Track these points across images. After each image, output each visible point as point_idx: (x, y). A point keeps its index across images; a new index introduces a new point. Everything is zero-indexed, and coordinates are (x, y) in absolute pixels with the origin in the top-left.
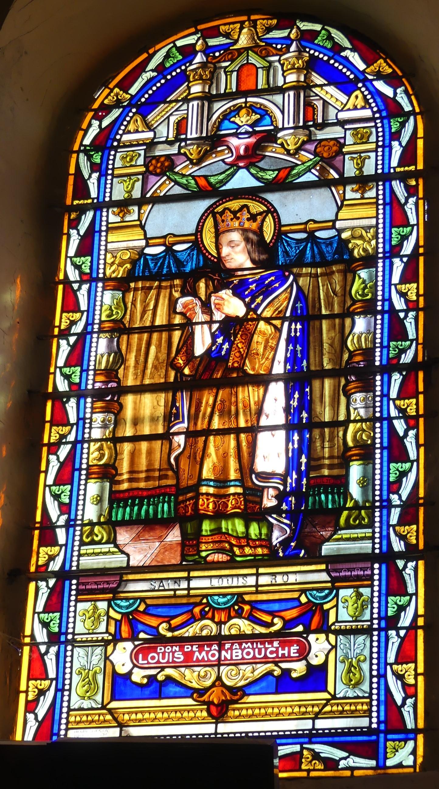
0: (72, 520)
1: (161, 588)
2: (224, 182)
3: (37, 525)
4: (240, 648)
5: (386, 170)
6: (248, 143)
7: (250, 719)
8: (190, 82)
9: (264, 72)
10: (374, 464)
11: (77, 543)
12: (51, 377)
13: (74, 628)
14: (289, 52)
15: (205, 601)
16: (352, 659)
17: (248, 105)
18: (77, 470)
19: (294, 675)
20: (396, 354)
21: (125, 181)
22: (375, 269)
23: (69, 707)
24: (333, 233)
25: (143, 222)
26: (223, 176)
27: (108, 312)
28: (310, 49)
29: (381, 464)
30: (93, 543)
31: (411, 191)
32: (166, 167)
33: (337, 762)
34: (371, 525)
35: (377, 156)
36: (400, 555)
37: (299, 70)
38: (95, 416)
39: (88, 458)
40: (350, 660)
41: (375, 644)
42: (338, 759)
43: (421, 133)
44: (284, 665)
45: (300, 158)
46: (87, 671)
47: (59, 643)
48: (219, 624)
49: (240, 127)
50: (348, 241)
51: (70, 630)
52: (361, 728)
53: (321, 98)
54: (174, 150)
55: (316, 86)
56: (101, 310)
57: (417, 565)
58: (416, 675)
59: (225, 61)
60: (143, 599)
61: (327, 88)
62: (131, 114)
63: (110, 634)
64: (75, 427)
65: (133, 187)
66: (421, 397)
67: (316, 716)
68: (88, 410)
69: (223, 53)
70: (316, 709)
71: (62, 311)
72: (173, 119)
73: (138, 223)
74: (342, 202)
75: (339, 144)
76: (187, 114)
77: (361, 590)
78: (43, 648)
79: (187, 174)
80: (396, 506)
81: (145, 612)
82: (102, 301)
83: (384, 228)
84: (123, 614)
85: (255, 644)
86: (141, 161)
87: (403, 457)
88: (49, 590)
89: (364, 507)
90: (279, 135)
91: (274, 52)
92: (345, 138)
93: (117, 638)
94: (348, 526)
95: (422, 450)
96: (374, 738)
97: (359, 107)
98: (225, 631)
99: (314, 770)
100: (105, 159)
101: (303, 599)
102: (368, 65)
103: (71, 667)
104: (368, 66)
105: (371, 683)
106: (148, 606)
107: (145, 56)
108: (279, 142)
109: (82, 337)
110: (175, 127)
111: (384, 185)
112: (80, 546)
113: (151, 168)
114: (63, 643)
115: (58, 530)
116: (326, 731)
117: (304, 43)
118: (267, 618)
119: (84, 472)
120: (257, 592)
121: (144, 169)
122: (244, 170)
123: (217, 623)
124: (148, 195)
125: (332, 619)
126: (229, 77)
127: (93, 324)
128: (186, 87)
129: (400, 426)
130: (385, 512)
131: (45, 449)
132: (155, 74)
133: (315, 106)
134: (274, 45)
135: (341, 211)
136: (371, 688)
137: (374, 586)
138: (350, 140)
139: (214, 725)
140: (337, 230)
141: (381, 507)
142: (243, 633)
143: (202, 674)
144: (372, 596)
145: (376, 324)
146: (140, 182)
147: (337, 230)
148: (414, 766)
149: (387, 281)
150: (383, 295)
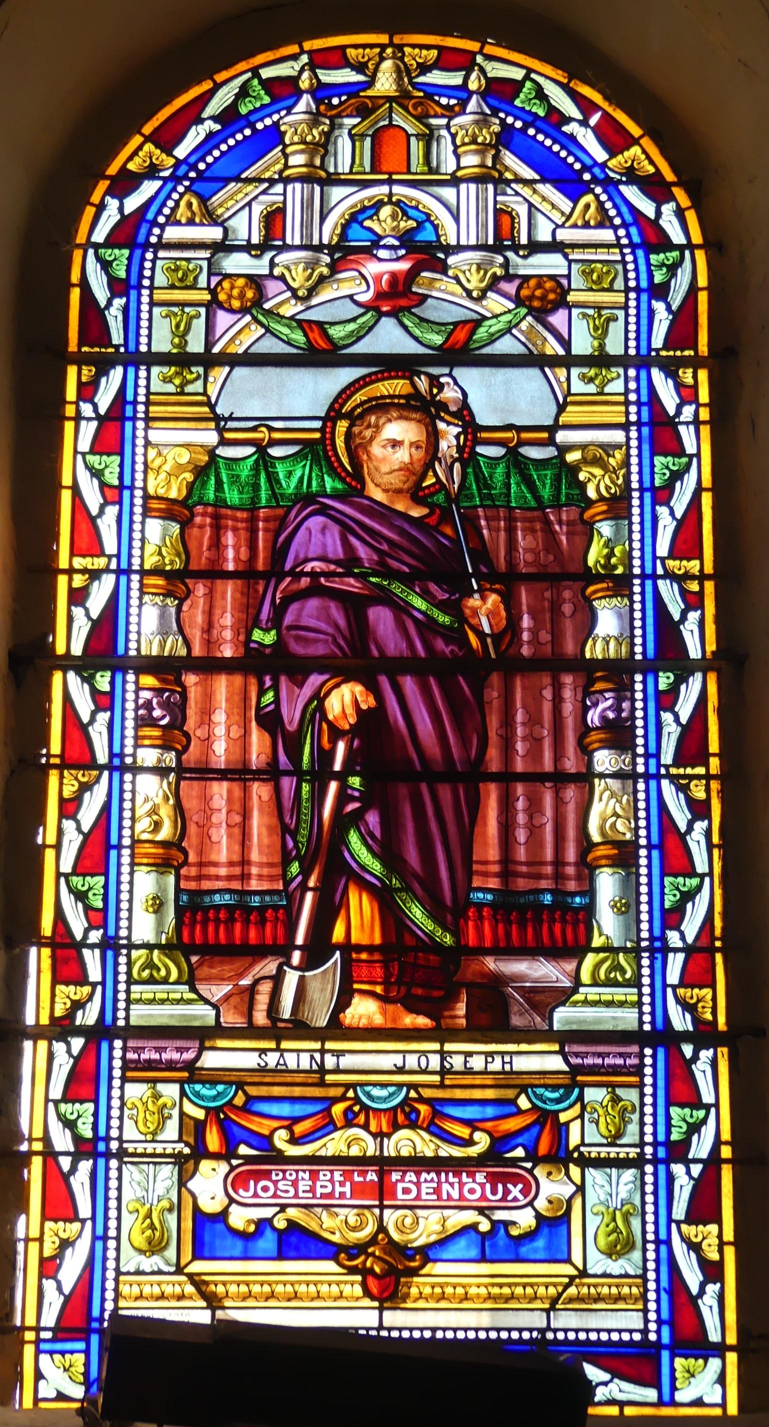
5: (644, 351)
9: (421, 143)
13: (120, 1128)
14: (463, 112)
17: (394, 199)
18: (114, 847)
21: (176, 315)
26: (352, 327)
29: (649, 875)
30: (152, 981)
35: (627, 315)
36: (685, 1036)
39: (132, 828)
43: (702, 281)
44: (499, 1215)
46: (148, 1206)
47: (95, 1155)
48: (379, 1135)
51: (114, 1133)
53: (525, 199)
54: (260, 267)
55: (519, 180)
57: (715, 1054)
58: (722, 1244)
61: (539, 187)
64: (99, 988)
68: (129, 742)
69: (346, 101)
70: (552, 1291)
72: (257, 209)
73: (204, 398)
74: (565, 398)
76: (285, 202)
78: (65, 1163)
80: (676, 950)
84: (208, 1110)
86: (203, 281)
89: (624, 950)
91: (438, 110)
92: (568, 277)
93: (200, 1152)
97: (592, 223)
98: (390, 1150)
100: (135, 266)
101: (523, 1103)
103: (119, 1199)
104: (612, 154)
106: (250, 1099)
108: (450, 273)
113: (222, 297)
114: (102, 1155)
115: (86, 952)
118: (463, 1132)
121: (209, 297)
123: (375, 1136)
124: (216, 350)
125: (574, 1140)
126: (357, 144)
128: (280, 154)
132: (218, 127)
133: (514, 213)
134: (437, 98)
136: (645, 1260)
137: (649, 1311)
138: (577, 281)
141: (652, 950)
142: (422, 1155)
144: (642, 1104)
150: (641, 481)
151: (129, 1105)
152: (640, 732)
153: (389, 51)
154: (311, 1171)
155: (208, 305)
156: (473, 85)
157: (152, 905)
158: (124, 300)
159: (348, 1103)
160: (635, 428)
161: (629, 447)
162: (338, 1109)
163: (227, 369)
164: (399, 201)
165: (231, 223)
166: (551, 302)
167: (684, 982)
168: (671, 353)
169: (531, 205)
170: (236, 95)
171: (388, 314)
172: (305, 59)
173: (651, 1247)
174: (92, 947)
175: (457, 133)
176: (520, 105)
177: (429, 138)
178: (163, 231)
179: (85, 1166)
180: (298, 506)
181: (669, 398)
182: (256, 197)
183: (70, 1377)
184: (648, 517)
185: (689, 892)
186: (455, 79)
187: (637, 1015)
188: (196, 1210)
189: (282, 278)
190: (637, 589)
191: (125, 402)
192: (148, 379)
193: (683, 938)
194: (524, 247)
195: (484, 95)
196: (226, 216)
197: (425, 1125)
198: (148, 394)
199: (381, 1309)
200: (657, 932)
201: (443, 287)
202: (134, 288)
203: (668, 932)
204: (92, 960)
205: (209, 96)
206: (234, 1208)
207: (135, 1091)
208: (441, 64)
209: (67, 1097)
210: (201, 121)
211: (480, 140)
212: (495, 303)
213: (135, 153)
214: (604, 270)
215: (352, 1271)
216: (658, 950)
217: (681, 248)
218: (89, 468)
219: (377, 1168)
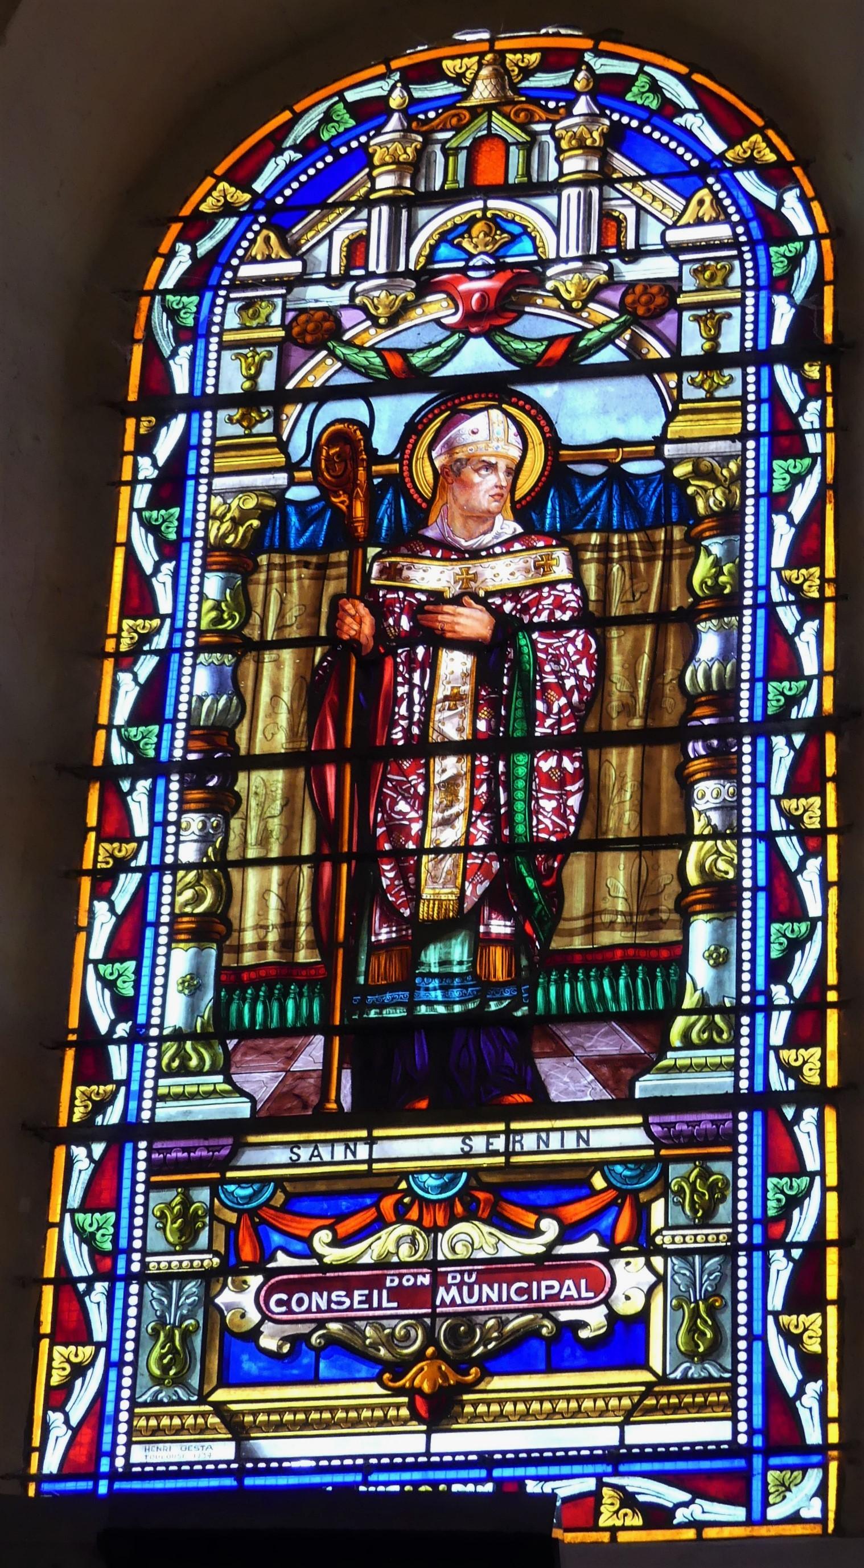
1: (315, 1160)
8: (373, 167)
10: (740, 920)
11: (150, 1073)
12: (53, 1234)
13: (144, 1238)
14: (570, 114)
15: (403, 1185)
16: (696, 1302)
17: (489, 214)
18: (151, 924)
19: (584, 1334)
20: (781, 707)
21: (246, 357)
24: (657, 466)
25: (285, 437)
28: (613, 111)
31: (811, 390)
32: (327, 331)
33: (670, 1512)
34: (734, 1043)
35: (744, 314)
36: (785, 1097)
37: (589, 150)
38: (186, 818)
39: (172, 904)
40: (693, 1305)
42: (670, 1505)
44: (564, 1316)
45: (592, 317)
49: (472, 256)
50: (685, 483)
51: (137, 1244)
52: (718, 1444)
56: (199, 612)
60: (279, 1181)
61: (647, 184)
62: (256, 227)
65: (259, 372)
66: (830, 788)
68: (173, 806)
70: (626, 1402)
71: (76, 1083)
73: (273, 439)
74: (675, 405)
75: (670, 288)
76: (368, 229)
79: (367, 345)
80: (781, 1008)
81: (287, 1208)
83: (757, 459)
87: (795, 911)
88: (93, 1165)
89: (721, 1009)
90: (549, 273)
92: (680, 278)
94: (688, 1044)
95: (833, 893)
96: (739, 1463)
101: (598, 1182)
102: (731, 146)
104: (731, 146)
107: (287, 115)
108: (549, 285)
110: (344, 254)
111: (753, 744)
112: (156, 1079)
115: (112, 1049)
116: (648, 1450)
117: (603, 100)
119: (164, 930)
121: (282, 334)
122: (482, 341)
124: (290, 386)
125: (657, 1220)
126: (451, 159)
129: (790, 850)
131: (86, 883)
132: (299, 156)
134: (543, 103)
135: (671, 424)
138: (689, 282)
140: (666, 461)
143: (399, 1332)
144: (736, 1177)
146: (275, 360)
147: (666, 461)
149: (762, 562)
152: (747, 759)
153: (489, 57)
160: (745, 830)
161: (745, 459)
162: (387, 1204)
163: (299, 407)
164: (495, 216)
169: (639, 208)
170: (320, 121)
171: (476, 335)
172: (397, 76)
181: (792, 395)
182: (337, 227)
184: (763, 527)
185: (794, 696)
186: (561, 79)
187: (732, 1079)
188: (225, 1328)
195: (593, 94)
199: (428, 1433)
203: (772, 986)
205: (287, 128)
209: (85, 1207)
210: (281, 152)
211: (589, 142)
212: (599, 312)
213: (209, 194)
215: (398, 1392)
216: (760, 1009)
217: (806, 240)
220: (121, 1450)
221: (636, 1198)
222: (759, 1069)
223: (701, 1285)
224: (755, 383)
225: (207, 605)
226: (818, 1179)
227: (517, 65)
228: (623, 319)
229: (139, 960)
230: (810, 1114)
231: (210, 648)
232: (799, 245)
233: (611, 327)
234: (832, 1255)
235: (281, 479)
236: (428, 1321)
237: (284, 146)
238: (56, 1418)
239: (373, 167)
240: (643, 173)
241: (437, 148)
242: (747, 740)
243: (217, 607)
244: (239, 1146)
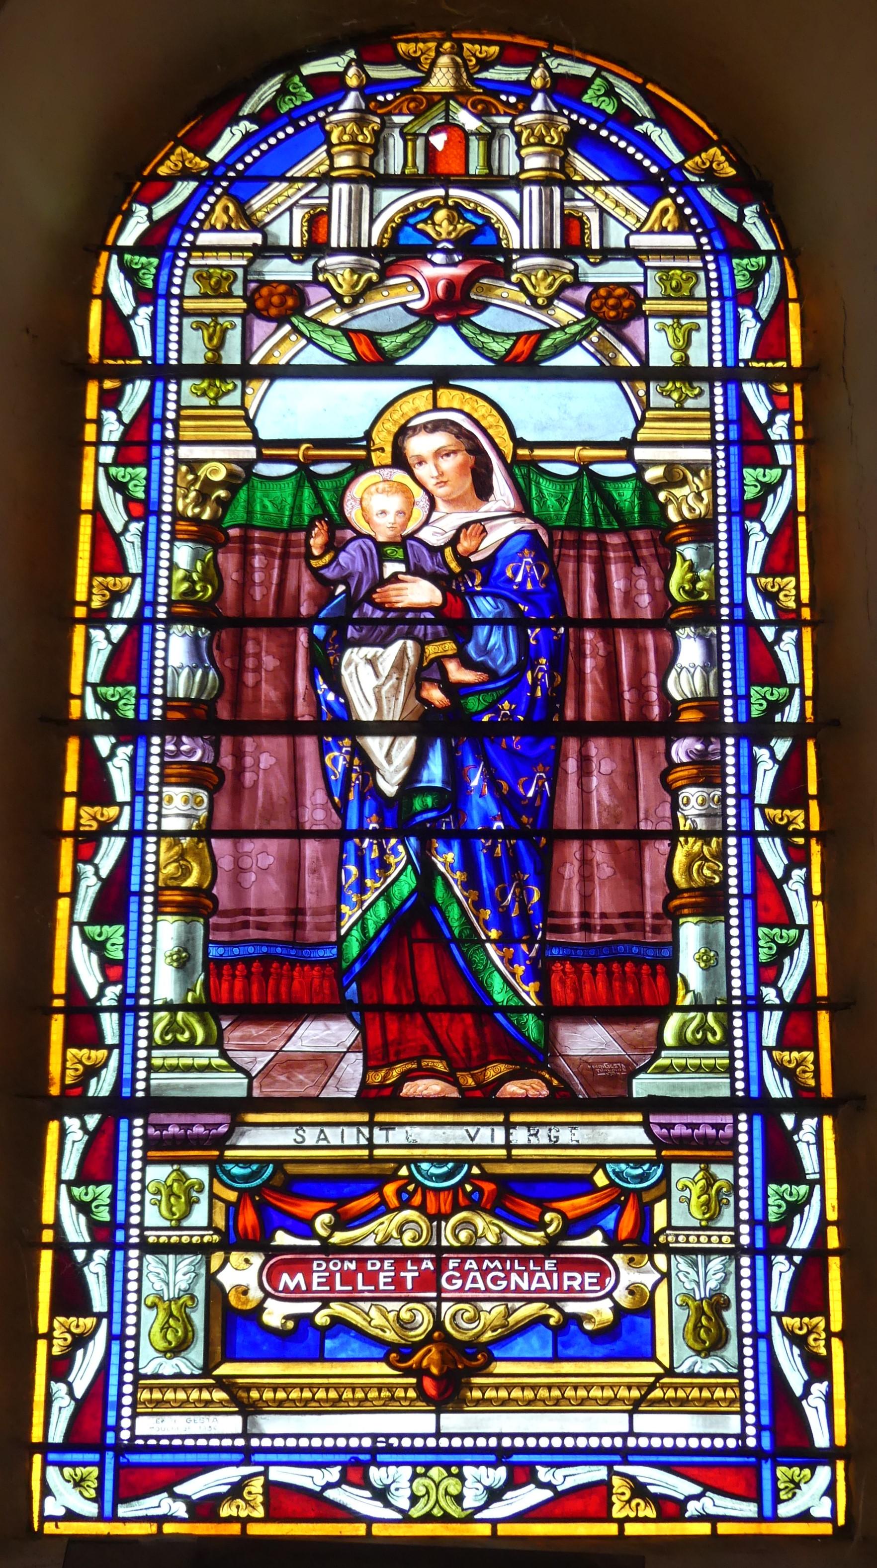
0: (131, 996)
2: (409, 348)
3: (58, 1003)
4: (480, 1270)
5: (730, 362)
6: (453, 276)
7: (505, 1405)
13: (141, 1214)
14: (528, 111)
15: (404, 1172)
19: (588, 1327)
21: (208, 326)
22: (712, 545)
23: (135, 1372)
24: (628, 469)
26: (404, 337)
27: (185, 586)
30: (175, 1045)
32: (291, 308)
34: (727, 1043)
35: (710, 326)
36: (784, 1105)
41: (735, 932)
44: (571, 1308)
51: (135, 1220)
53: (597, 205)
54: (302, 272)
55: (586, 182)
59: (401, 113)
61: (609, 189)
63: (217, 1231)
66: (814, 806)
67: (635, 1407)
70: (635, 1394)
72: (298, 213)
73: (242, 413)
76: (329, 206)
77: (715, 1169)
78: (80, 1255)
80: (772, 1008)
82: (170, 560)
85: (508, 1262)
86: (238, 289)
91: (501, 109)
92: (644, 284)
94: (683, 1044)
97: (670, 229)
99: (637, 1520)
101: (600, 1179)
102: (688, 156)
104: (688, 156)
105: (741, 1346)
108: (514, 278)
109: (136, 624)
110: (305, 228)
113: (260, 304)
120: (509, 1159)
121: (244, 305)
123: (431, 1218)
124: (255, 361)
125: (660, 1221)
126: (410, 144)
127: (154, 604)
128: (324, 155)
130: (751, 1016)
131: (67, 847)
132: (254, 127)
136: (741, 1357)
138: (654, 289)
139: (433, 1416)
141: (745, 1009)
145: (728, 937)
146: (239, 329)
148: (833, 1520)
149: (737, 570)
151: (152, 1188)
154: (357, 1260)
155: (244, 315)
156: (537, 83)
157: (177, 960)
158: (151, 308)
159: (401, 1182)
160: (730, 829)
162: (390, 1190)
163: (267, 382)
164: (457, 204)
165: (271, 228)
166: (625, 309)
167: (784, 1043)
168: (762, 364)
169: (602, 211)
170: (277, 91)
171: (444, 323)
173: (748, 1341)
174: (109, 1009)
175: (521, 132)
176: (588, 101)
177: (490, 138)
178: (196, 237)
179: (101, 1255)
180: (352, 147)
181: (761, 409)
183: (81, 1493)
186: (518, 74)
189: (326, 284)
190: (734, 912)
191: (153, 420)
192: (178, 393)
193: (780, 994)
194: (595, 252)
196: (267, 220)
197: (488, 1207)
198: (179, 408)
200: (750, 990)
201: (505, 295)
202: (162, 297)
204: (109, 1023)
206: (270, 1303)
207: (158, 1173)
208: (503, 60)
210: (236, 120)
211: (547, 139)
212: (564, 313)
214: (684, 277)
215: (407, 1373)
218: (86, 939)
219: (433, 1256)
220: (126, 1423)
221: (640, 1198)
222: (753, 1067)
223: (706, 1283)
224: (740, 978)
225: (179, 575)
226: (797, 691)
227: (474, 55)
228: (588, 321)
229: (126, 922)
230: (809, 1124)
231: (183, 619)
232: (762, 260)
233: (577, 328)
234: (834, 1264)
235: (250, 453)
236: (434, 1304)
237: (241, 114)
238: (59, 1388)
239: (331, 145)
240: (607, 179)
241: (396, 133)
242: (730, 741)
243: (187, 578)
244: (237, 1124)
